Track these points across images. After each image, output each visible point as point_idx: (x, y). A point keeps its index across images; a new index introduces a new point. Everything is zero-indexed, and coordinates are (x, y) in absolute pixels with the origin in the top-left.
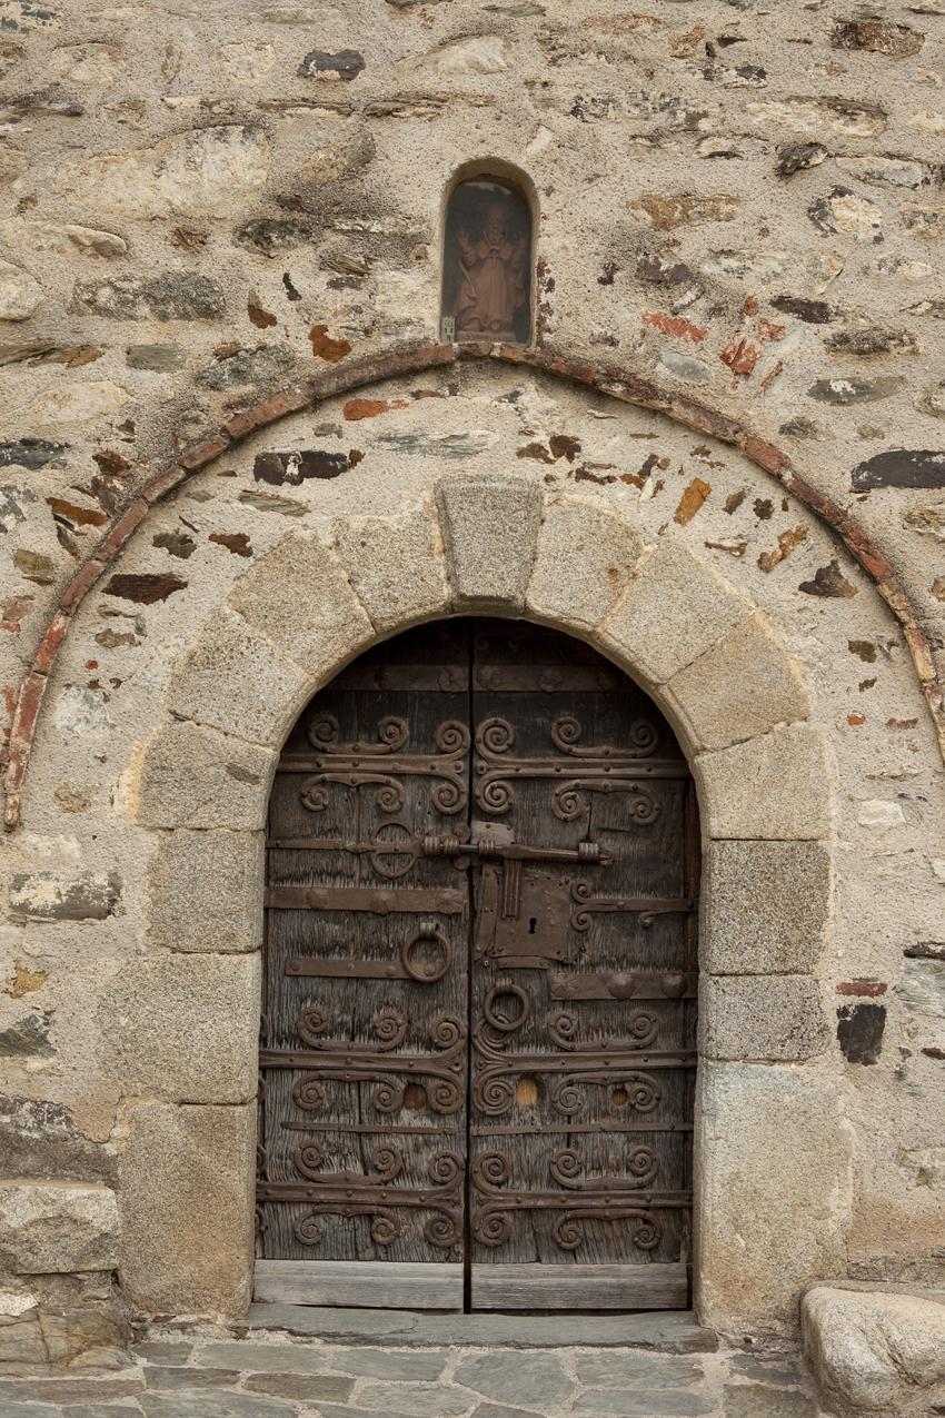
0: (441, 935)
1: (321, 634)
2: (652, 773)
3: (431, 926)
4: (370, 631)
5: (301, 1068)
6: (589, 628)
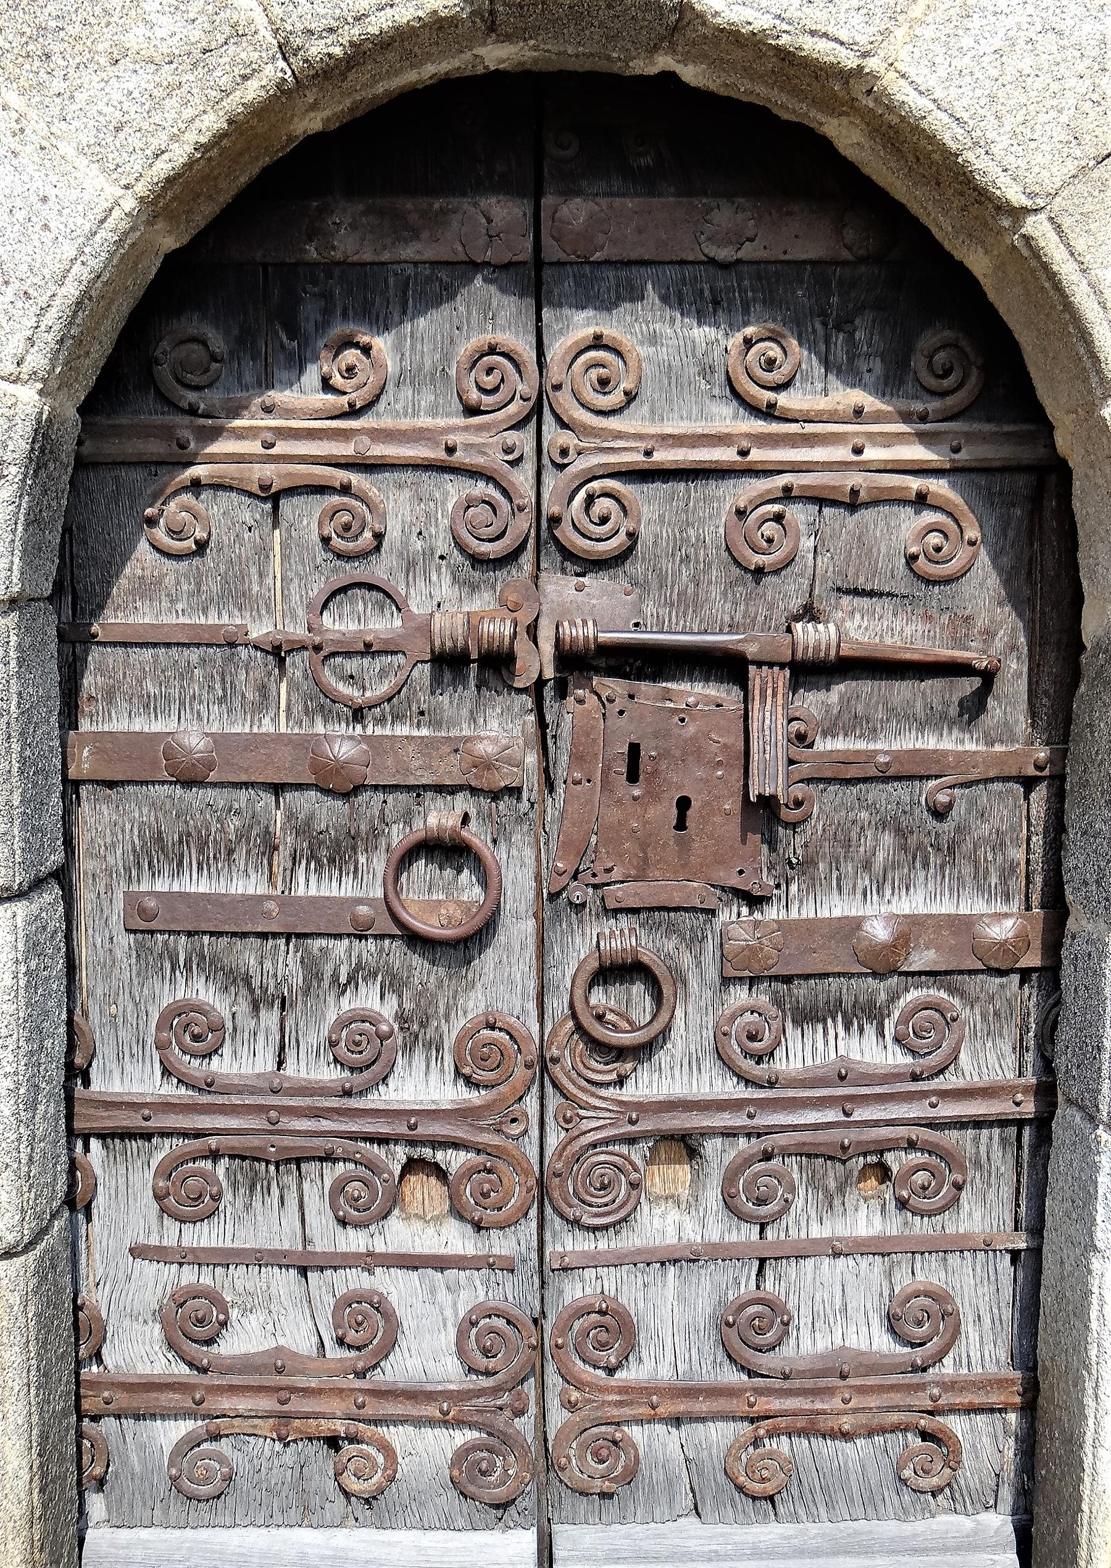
0: (476, 835)
1: (143, 80)
2: (963, 455)
3: (451, 821)
4: (275, 71)
5: (165, 1134)
6: (850, 61)
